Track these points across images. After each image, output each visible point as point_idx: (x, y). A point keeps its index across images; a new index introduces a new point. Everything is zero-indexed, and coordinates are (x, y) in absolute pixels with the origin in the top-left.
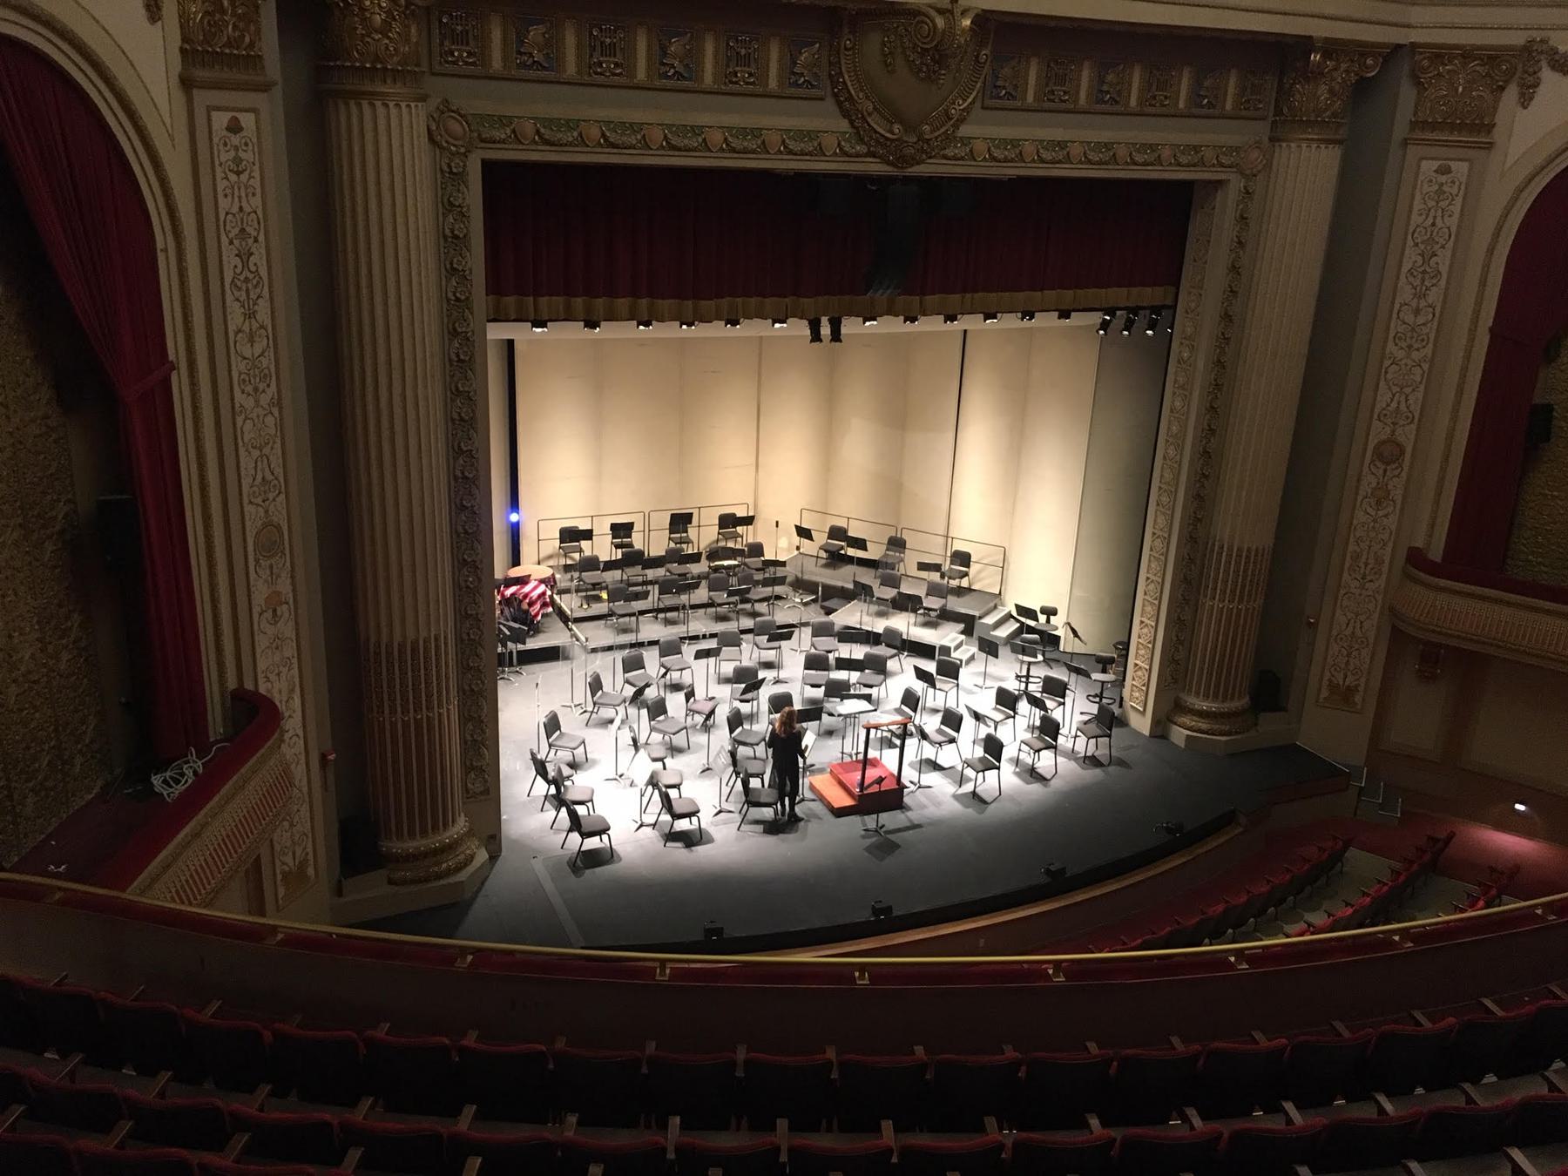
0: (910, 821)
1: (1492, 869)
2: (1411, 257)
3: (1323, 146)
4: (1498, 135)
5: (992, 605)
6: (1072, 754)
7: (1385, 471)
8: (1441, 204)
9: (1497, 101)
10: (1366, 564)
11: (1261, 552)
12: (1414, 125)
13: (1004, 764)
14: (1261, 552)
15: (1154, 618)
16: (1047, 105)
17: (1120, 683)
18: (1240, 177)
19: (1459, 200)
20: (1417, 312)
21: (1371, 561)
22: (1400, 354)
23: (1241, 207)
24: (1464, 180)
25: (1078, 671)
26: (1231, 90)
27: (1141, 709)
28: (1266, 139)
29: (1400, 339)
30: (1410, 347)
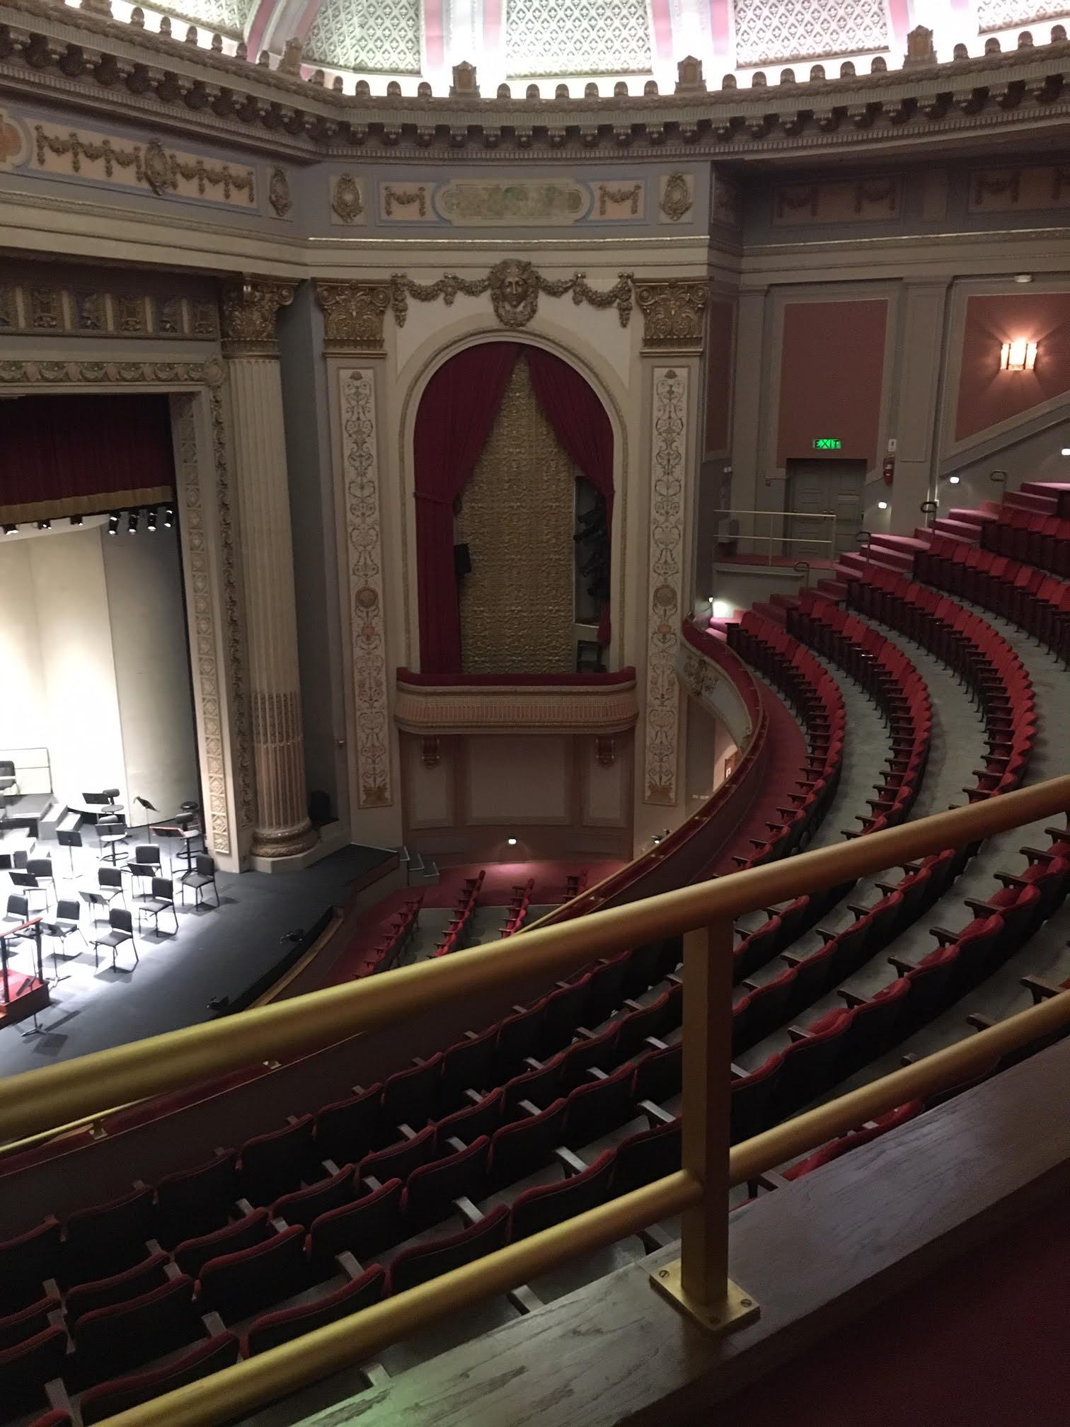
0: (66, 1012)
1: (516, 888)
2: (348, 447)
3: (267, 361)
4: (387, 347)
5: (47, 805)
6: (186, 909)
7: (367, 613)
8: (361, 403)
9: (381, 321)
10: (370, 688)
11: (289, 697)
12: (328, 342)
13: (135, 933)
14: (289, 697)
15: (221, 771)
16: (199, 336)
17: (202, 836)
18: (208, 389)
19: (372, 399)
20: (362, 487)
21: (373, 685)
22: (358, 521)
23: (215, 413)
24: (372, 383)
25: (169, 834)
26: (186, 317)
27: (227, 852)
28: (220, 358)
29: (355, 509)
30: (363, 514)
